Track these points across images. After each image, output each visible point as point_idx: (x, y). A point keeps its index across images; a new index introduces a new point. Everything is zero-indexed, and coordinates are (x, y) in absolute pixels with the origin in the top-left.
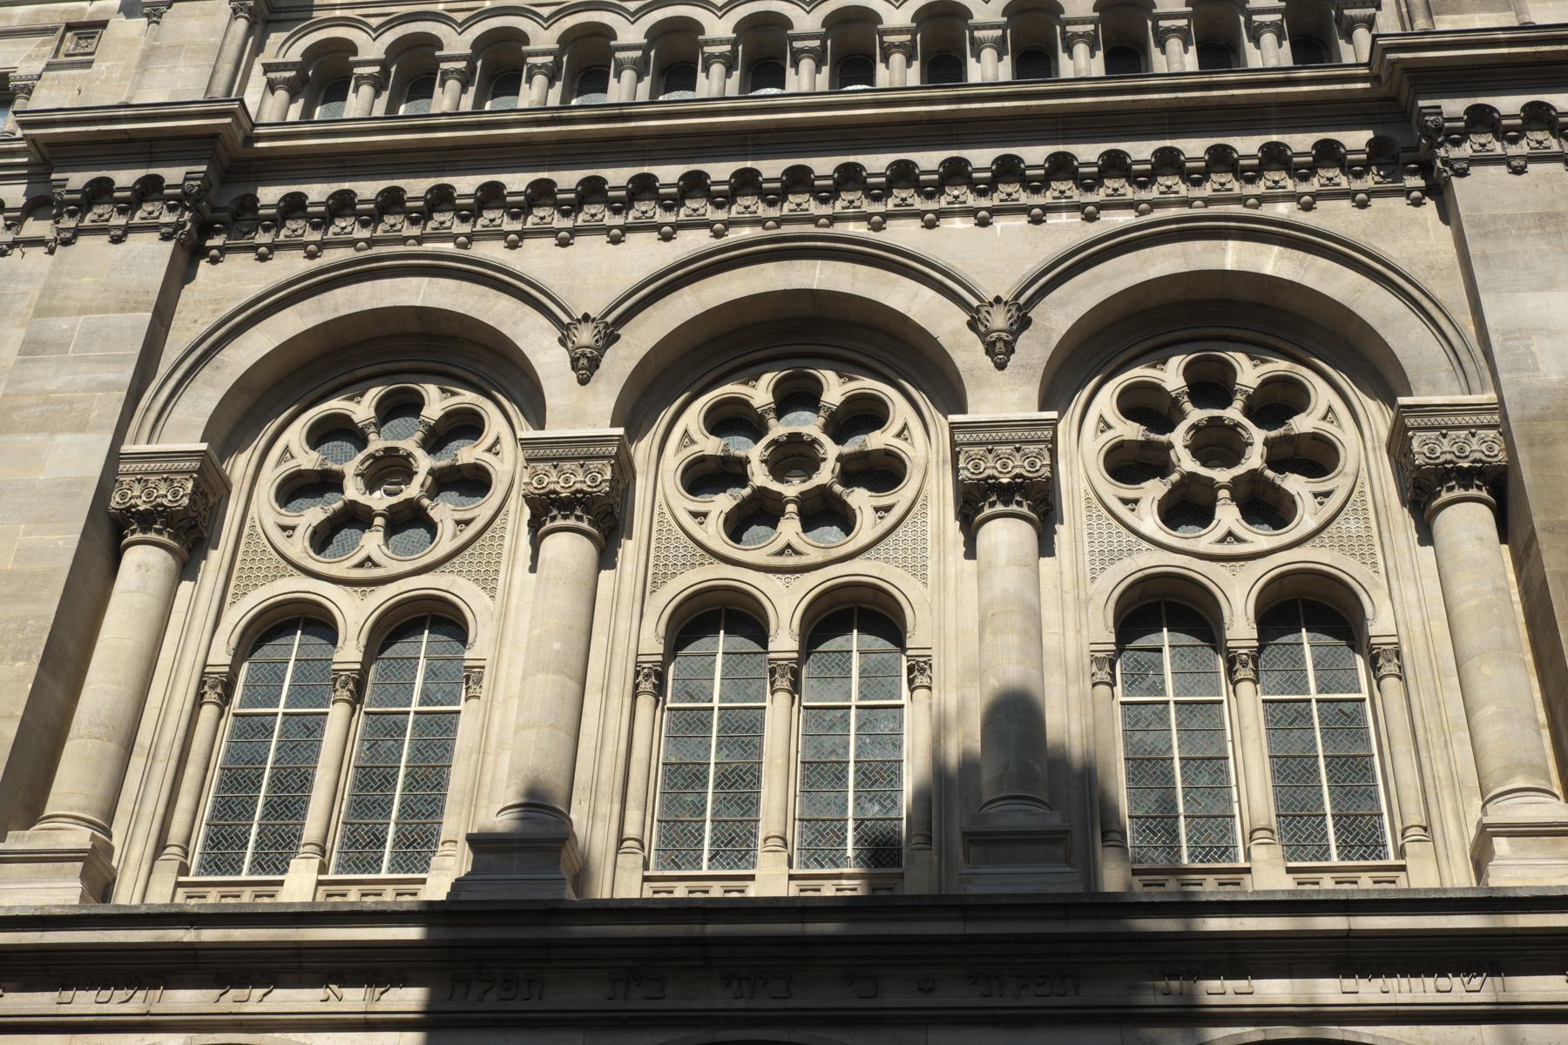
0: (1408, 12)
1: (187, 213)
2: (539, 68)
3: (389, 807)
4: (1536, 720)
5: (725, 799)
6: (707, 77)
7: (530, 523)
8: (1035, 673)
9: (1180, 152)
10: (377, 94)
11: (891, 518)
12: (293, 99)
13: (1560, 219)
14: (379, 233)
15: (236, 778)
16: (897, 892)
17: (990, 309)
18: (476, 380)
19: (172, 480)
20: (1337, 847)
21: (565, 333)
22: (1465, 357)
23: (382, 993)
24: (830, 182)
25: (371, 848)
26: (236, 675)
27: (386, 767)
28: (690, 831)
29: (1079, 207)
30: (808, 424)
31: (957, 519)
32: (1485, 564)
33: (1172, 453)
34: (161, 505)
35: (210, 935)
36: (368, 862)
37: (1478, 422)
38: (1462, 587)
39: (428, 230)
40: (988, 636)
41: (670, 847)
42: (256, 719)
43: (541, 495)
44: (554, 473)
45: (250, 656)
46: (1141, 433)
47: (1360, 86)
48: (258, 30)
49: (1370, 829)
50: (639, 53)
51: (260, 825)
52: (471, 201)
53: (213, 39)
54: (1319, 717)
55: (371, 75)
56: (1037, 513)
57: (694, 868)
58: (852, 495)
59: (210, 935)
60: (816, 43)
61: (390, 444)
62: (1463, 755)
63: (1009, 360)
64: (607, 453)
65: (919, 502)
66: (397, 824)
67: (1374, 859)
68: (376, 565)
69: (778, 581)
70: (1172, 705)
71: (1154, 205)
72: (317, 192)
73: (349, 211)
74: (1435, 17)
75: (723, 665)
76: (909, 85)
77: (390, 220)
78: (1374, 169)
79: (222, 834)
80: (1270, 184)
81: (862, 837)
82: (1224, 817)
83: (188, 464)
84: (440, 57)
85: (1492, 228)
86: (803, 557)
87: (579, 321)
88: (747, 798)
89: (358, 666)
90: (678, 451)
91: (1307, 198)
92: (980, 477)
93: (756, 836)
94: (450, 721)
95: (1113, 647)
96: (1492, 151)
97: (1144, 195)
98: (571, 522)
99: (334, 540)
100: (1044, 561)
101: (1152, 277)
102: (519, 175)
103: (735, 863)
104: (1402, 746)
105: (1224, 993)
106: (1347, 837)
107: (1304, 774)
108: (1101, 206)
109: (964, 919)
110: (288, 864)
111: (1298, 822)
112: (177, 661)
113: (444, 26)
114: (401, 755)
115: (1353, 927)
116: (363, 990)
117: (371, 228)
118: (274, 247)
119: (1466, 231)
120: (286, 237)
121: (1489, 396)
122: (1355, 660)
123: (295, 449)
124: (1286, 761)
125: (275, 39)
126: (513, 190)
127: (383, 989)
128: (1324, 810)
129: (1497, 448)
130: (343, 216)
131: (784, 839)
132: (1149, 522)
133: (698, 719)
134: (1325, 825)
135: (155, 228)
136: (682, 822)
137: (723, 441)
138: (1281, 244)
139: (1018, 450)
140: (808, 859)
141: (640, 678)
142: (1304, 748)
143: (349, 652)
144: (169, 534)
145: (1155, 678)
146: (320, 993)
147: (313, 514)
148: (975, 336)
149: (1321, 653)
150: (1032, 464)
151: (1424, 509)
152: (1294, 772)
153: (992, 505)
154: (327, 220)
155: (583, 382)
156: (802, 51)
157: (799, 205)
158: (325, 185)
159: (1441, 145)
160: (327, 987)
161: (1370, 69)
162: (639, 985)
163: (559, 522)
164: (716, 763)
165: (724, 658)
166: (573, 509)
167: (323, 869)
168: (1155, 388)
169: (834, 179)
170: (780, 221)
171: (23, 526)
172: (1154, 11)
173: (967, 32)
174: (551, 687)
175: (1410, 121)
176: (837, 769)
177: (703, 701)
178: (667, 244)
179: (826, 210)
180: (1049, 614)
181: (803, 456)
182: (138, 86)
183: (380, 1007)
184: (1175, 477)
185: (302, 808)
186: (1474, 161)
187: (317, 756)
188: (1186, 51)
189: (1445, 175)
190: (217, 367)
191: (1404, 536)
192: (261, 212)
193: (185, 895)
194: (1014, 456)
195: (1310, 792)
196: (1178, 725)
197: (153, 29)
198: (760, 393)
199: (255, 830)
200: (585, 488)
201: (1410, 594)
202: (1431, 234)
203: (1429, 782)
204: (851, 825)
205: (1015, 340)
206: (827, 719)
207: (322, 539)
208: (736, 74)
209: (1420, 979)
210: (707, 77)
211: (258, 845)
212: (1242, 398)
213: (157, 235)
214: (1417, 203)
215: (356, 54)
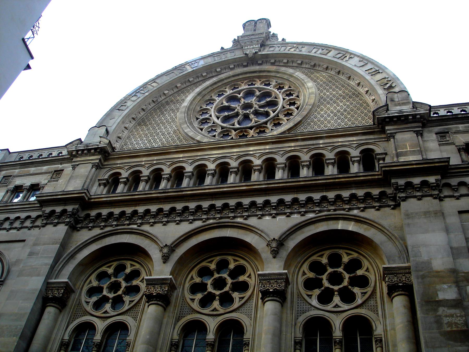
13: (430, 213)
46: (314, 275)
55: (124, 181)
90: (302, 277)
113: (143, 168)
132: (315, 302)
135: (64, 223)
168: (320, 263)
171: (21, 301)
182: (66, 186)
184: (323, 288)
200: (160, 293)
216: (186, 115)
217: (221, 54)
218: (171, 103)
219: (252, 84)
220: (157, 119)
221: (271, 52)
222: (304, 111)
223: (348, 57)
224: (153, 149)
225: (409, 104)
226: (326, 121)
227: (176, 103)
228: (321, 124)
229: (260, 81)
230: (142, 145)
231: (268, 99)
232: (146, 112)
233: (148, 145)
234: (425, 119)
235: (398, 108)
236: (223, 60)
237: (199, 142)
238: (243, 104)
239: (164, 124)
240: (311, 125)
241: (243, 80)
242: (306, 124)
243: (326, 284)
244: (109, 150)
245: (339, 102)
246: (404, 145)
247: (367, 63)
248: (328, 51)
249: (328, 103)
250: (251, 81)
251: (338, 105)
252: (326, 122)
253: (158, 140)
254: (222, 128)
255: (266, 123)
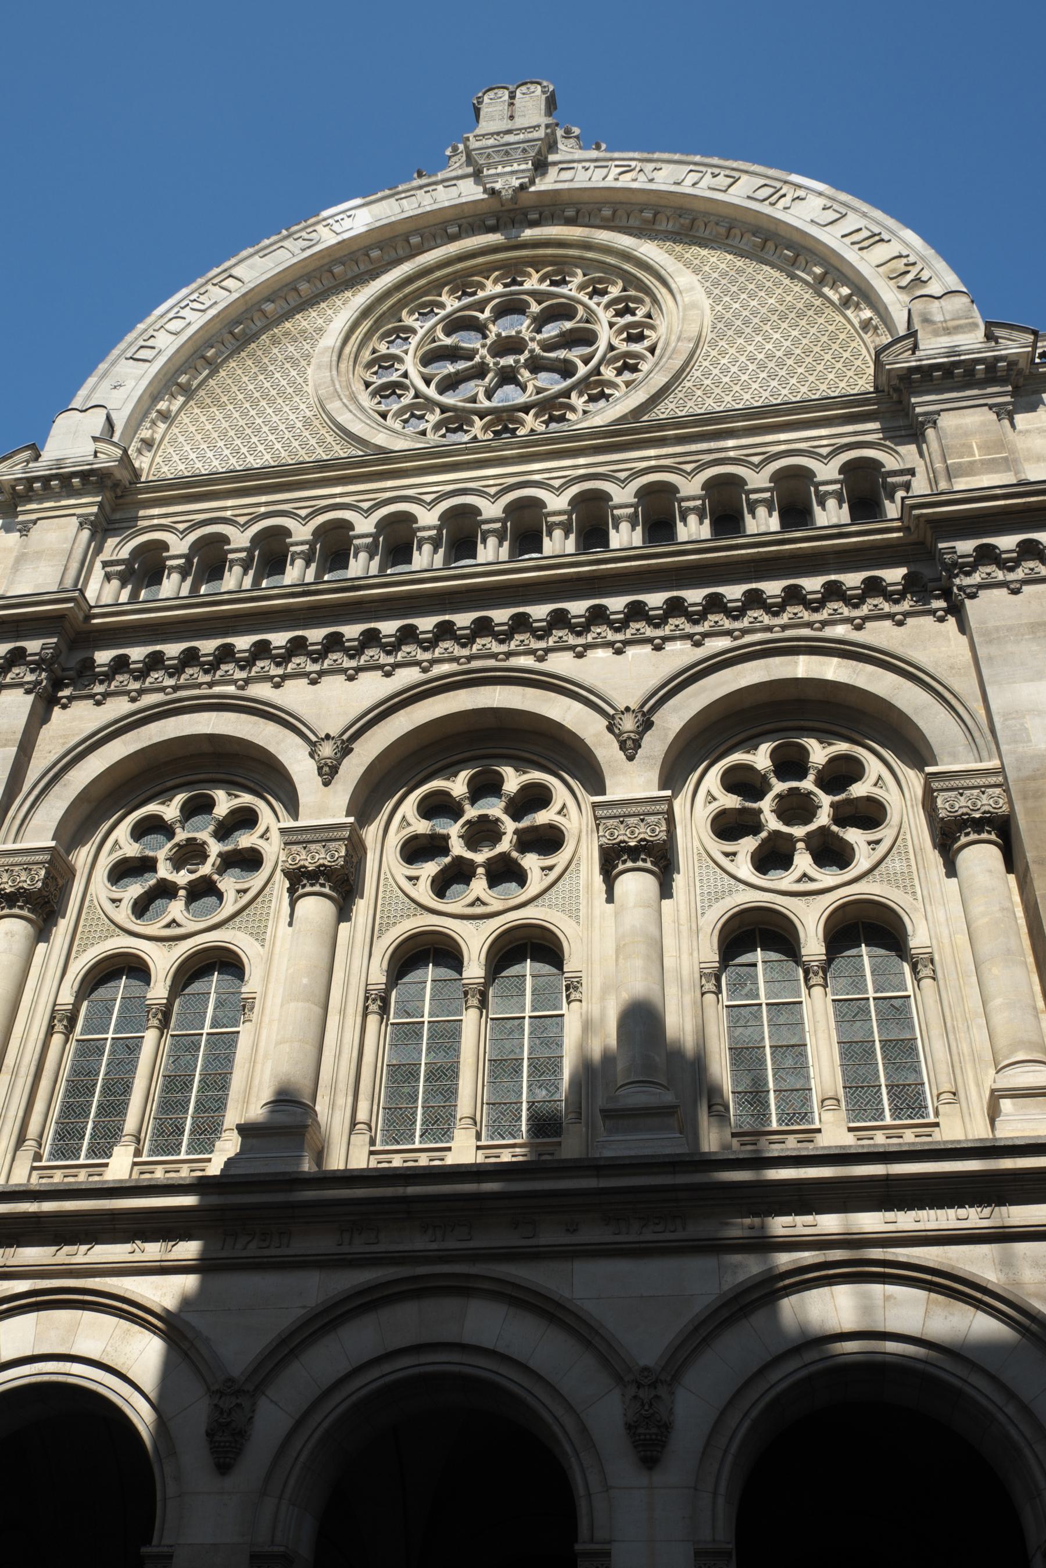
0: (934, 477)
1: (44, 673)
2: (299, 554)
3: (187, 1105)
4: (1035, 1008)
5: (432, 1090)
6: (420, 554)
7: (289, 890)
8: (657, 988)
9: (763, 592)
10: (184, 579)
11: (553, 875)
12: (123, 585)
14: (182, 681)
15: (77, 1088)
16: (556, 1157)
17: (622, 716)
18: (252, 785)
19: (30, 870)
20: (890, 1110)
21: (313, 747)
22: (976, 734)
23: (173, 1246)
24: (583, 620)
25: (174, 1136)
26: (78, 1011)
27: (185, 1075)
28: (406, 1115)
29: (689, 637)
30: (494, 808)
31: (601, 874)
32: (993, 890)
33: (762, 816)
34: (22, 888)
35: (48, 1206)
36: (171, 1147)
37: (987, 783)
38: (977, 908)
39: (217, 677)
40: (621, 960)
41: (392, 1128)
42: (92, 1043)
43: (294, 869)
44: (304, 852)
45: (89, 996)
46: (739, 802)
47: (895, 535)
48: (99, 536)
49: (915, 1095)
50: (370, 540)
51: (94, 1122)
52: (247, 654)
53: (65, 546)
54: (876, 1011)
55: (179, 565)
56: (658, 867)
57: (409, 1143)
58: (525, 859)
59: (48, 1206)
60: (498, 525)
61: (190, 835)
62: (980, 1036)
63: (637, 753)
64: (342, 837)
65: (574, 862)
66: (193, 1118)
67: (918, 1118)
68: (179, 925)
69: (470, 926)
70: (764, 1006)
71: (745, 632)
72: (137, 653)
73: (161, 666)
74: (953, 480)
75: (432, 989)
76: (567, 552)
77: (189, 671)
78: (909, 596)
79: (67, 1130)
80: (831, 611)
81: (533, 1115)
82: (804, 1090)
83: (41, 857)
84: (227, 550)
85: (995, 636)
86: (489, 907)
87: (322, 739)
88: (449, 1089)
89: (165, 1001)
90: (398, 831)
91: (858, 621)
92: (614, 842)
93: (455, 1118)
94: (232, 1040)
95: (824, 958)
96: (996, 578)
97: (737, 625)
98: (317, 888)
99: (151, 908)
100: (666, 903)
101: (743, 686)
102: (281, 634)
103: (439, 1138)
104: (936, 1030)
105: (795, 1226)
106: (898, 1102)
107: (864, 1055)
108: (706, 635)
109: (598, 1176)
110: (214, 1146)
111: (860, 1092)
112: (35, 1003)
113: (231, 527)
114: (196, 1067)
115: (890, 1173)
116: (159, 1244)
117: (176, 677)
118: (106, 695)
119: (976, 639)
120: (366, 661)
121: (995, 763)
122: (903, 966)
123: (122, 842)
124: (851, 1046)
125: (111, 542)
126: (277, 645)
127: (174, 1243)
128: (879, 1082)
129: (1001, 801)
130: (156, 670)
131: (474, 1119)
132: (744, 869)
133: (413, 1031)
134: (881, 1094)
136: (400, 1108)
137: (431, 824)
138: (839, 656)
139: (642, 820)
140: (493, 1133)
141: (369, 1002)
142: (864, 1035)
143: (158, 991)
144: (29, 908)
145: (752, 986)
146: (128, 1247)
147: (135, 889)
148: (612, 736)
149: (877, 962)
150: (653, 831)
151: (950, 850)
152: (857, 1054)
153: (624, 862)
154: (145, 674)
155: (326, 784)
156: (489, 531)
157: (484, 645)
158: (143, 648)
159: (957, 576)
160: (134, 1242)
161: (902, 522)
162: (452, 1231)
163: (308, 889)
164: (426, 1064)
165: (432, 985)
166: (319, 879)
167: (138, 1153)
168: (749, 768)
169: (625, 614)
170: (470, 658)
172: (746, 487)
173: (676, 504)
174: (301, 1012)
175: (934, 559)
176: (515, 1064)
177: (417, 1017)
178: (389, 679)
179: (503, 648)
180: (669, 942)
181: (491, 831)
182: (12, 582)
183: (172, 1256)
184: (764, 834)
185: (124, 1108)
186: (981, 587)
187: (136, 1069)
188: (770, 515)
189: (960, 598)
190: (65, 785)
191: (935, 872)
192: (97, 670)
193: (38, 1176)
194: (639, 825)
195: (869, 1068)
196: (769, 1021)
197: (23, 540)
198: (458, 786)
199: (90, 1126)
200: (326, 863)
201: (941, 915)
202: (952, 643)
203: (956, 1058)
204: (525, 1106)
205: (641, 738)
206: (508, 1027)
207: (141, 908)
208: (506, 544)
209: (944, 1211)
210: (420, 554)
211: (92, 1137)
212: (814, 772)
213: (22, 690)
214: (941, 620)
215: (229, 543)
216: (334, 372)
217: (418, 192)
218: (284, 341)
219: (514, 282)
220: (251, 387)
221: (566, 186)
222: (674, 356)
223: (789, 198)
224: (249, 474)
225: (974, 330)
226: (737, 384)
227: (301, 339)
228: (723, 394)
229: (537, 272)
230: (216, 463)
231: (568, 325)
232: (213, 367)
233: (233, 461)
234: (1020, 372)
235: (945, 342)
236: (428, 209)
237: (381, 450)
238: (495, 341)
239: (271, 402)
240: (695, 398)
241: (486, 271)
242: (680, 395)
243: (772, 823)
244: (123, 475)
245: (770, 331)
246: (964, 444)
247: (846, 214)
248: (732, 180)
249: (740, 333)
250: (513, 272)
251: (767, 338)
252: (737, 388)
253: (261, 448)
254: (444, 409)
255: (566, 393)
